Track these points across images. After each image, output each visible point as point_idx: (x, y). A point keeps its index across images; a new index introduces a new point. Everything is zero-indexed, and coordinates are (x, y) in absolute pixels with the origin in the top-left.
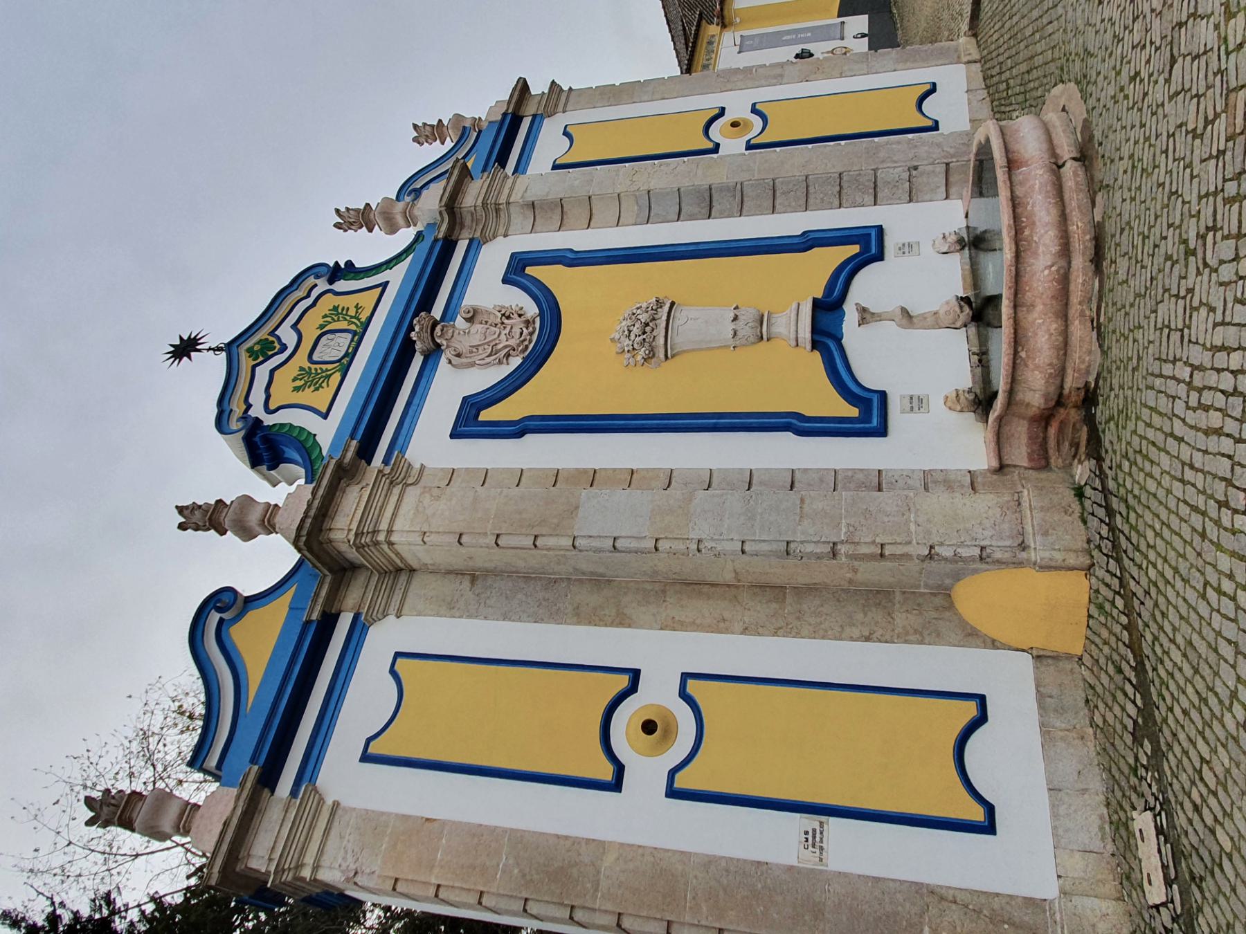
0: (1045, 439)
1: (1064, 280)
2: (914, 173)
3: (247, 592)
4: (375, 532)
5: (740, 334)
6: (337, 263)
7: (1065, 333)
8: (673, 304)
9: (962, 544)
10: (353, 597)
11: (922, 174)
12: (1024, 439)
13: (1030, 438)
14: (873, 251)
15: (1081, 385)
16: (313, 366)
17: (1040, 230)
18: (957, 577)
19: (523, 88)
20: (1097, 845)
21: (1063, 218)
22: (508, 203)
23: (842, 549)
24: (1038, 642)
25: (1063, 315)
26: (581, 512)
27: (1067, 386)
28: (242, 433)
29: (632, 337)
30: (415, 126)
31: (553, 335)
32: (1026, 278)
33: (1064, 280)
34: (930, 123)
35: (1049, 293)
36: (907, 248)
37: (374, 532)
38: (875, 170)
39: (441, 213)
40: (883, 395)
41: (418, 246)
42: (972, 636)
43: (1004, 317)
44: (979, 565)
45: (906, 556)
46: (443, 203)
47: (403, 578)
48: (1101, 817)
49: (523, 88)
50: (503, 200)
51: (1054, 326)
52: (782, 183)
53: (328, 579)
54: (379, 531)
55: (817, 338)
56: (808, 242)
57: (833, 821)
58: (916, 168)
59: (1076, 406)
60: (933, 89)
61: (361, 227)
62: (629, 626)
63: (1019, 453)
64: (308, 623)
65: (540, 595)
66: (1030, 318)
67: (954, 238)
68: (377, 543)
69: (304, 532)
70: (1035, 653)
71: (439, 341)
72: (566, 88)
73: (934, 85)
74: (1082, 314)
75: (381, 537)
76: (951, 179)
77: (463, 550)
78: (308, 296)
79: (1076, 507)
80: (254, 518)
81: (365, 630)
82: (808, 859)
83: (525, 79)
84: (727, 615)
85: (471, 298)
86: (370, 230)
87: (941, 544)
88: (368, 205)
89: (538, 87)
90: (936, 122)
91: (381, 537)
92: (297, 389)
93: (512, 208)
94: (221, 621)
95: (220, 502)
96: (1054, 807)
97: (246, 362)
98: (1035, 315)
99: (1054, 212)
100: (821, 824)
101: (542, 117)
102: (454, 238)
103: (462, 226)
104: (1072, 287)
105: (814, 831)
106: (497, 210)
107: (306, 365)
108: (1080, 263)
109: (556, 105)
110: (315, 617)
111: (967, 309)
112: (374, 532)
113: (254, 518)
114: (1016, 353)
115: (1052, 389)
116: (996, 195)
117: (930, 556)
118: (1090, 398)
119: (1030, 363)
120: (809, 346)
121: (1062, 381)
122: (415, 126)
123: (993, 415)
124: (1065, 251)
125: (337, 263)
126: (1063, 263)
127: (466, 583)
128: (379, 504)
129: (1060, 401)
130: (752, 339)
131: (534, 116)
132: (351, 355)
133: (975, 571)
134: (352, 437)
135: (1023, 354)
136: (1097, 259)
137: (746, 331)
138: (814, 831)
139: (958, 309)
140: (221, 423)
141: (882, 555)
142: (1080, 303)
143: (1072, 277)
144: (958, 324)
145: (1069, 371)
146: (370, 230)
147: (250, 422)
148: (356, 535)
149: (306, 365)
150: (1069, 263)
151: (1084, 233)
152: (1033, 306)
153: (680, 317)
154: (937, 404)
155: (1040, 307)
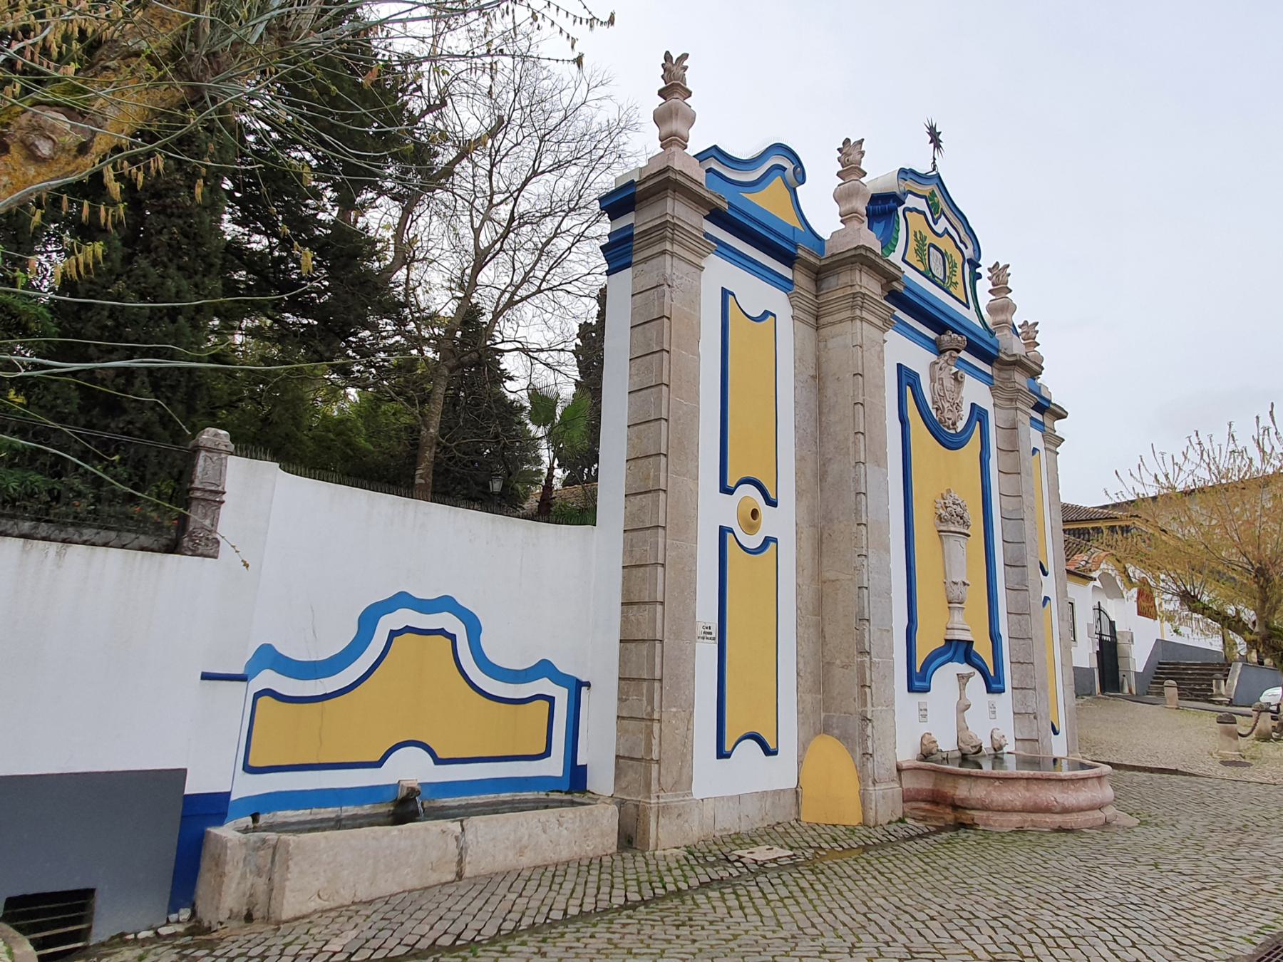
0: (917, 800)
1: (1048, 810)
2: (1032, 716)
3: (800, 190)
4: (672, 241)
5: (955, 587)
6: (980, 266)
7: (1013, 811)
8: (968, 536)
9: (873, 742)
10: (802, 279)
11: (1030, 722)
12: (917, 786)
13: (918, 790)
14: (994, 686)
15: (976, 821)
16: (926, 247)
17: (1074, 794)
18: (844, 738)
19: (1061, 415)
20: (718, 827)
21: (1081, 810)
22: (1017, 409)
23: (867, 659)
24: (806, 792)
25: (1025, 810)
26: (876, 468)
27: (972, 812)
28: (898, 192)
29: (955, 507)
30: (1036, 324)
31: (949, 444)
32: (1046, 785)
33: (1048, 810)
34: (727, 748)
35: (1038, 800)
36: (992, 708)
37: (672, 239)
38: (1035, 689)
39: (1015, 355)
40: (927, 690)
41: (987, 333)
42: (803, 747)
43: (1022, 772)
44: (859, 752)
45: (865, 704)
46: (1023, 359)
47: (812, 321)
48: (730, 830)
49: (1061, 415)
50: (1019, 405)
51: (1018, 803)
52: (1027, 620)
53: (818, 262)
54: (672, 244)
55: (954, 643)
56: (995, 638)
57: (714, 647)
58: (1035, 718)
59: (956, 819)
60: (768, 752)
61: (994, 285)
62: (797, 499)
63: (910, 783)
64: (796, 247)
65: (809, 431)
66: (1021, 788)
67: (1003, 743)
68: (853, 308)
69: (869, 254)
70: (799, 790)
71: (948, 353)
72: (1058, 450)
73: (775, 753)
74: (1025, 821)
75: (858, 312)
76: (1027, 743)
77: (849, 376)
78: (962, 242)
79: (894, 819)
80: (676, 126)
81: (785, 290)
82: (700, 630)
83: (1065, 417)
84: (805, 572)
85: (969, 380)
86: (990, 291)
87: (873, 727)
88: (1011, 291)
89: (1060, 426)
90: (728, 756)
91: (858, 312)
92: (915, 235)
93: (1013, 411)
94: (784, 169)
95: (689, 94)
96: (732, 797)
97: (925, 190)
98: (1023, 792)
99: (1084, 804)
100: (714, 639)
101: (1043, 431)
102: (995, 364)
103: (1000, 370)
104: (1041, 815)
105: (711, 633)
106: (1011, 400)
107: (927, 242)
108: (1058, 819)
109: (1050, 443)
110: (799, 251)
111: (974, 750)
112: (672, 239)
113: (676, 126)
114: (998, 779)
115: (973, 802)
116: (1069, 770)
117: (865, 719)
118: (960, 825)
119: (991, 788)
120: (949, 637)
121: (978, 809)
122: (1036, 324)
123: (922, 764)
124: (1066, 811)
125: (980, 266)
126: (1058, 809)
127: (812, 372)
128: (684, 242)
129: (955, 807)
130: (951, 596)
131: (1043, 424)
132: (932, 279)
133: (852, 751)
134: (906, 287)
135: (997, 783)
136: (1060, 830)
137: (956, 591)
138: (711, 633)
139: (974, 744)
140: (904, 173)
141: (864, 686)
142: (1032, 820)
143: (1047, 815)
144: (961, 744)
145: (984, 814)
146: (990, 291)
147: (902, 198)
148: (864, 294)
149: (927, 242)
150: (1057, 813)
151: (1075, 822)
152: (1028, 790)
153: (962, 540)
154: (923, 729)
155: (1028, 794)
